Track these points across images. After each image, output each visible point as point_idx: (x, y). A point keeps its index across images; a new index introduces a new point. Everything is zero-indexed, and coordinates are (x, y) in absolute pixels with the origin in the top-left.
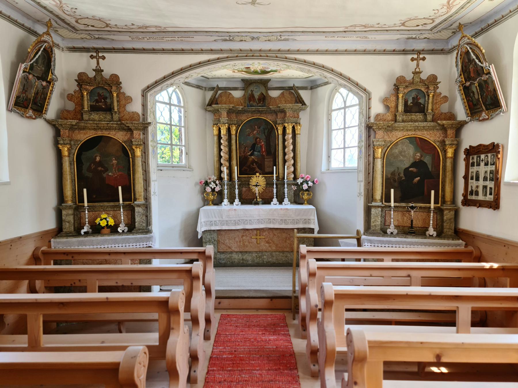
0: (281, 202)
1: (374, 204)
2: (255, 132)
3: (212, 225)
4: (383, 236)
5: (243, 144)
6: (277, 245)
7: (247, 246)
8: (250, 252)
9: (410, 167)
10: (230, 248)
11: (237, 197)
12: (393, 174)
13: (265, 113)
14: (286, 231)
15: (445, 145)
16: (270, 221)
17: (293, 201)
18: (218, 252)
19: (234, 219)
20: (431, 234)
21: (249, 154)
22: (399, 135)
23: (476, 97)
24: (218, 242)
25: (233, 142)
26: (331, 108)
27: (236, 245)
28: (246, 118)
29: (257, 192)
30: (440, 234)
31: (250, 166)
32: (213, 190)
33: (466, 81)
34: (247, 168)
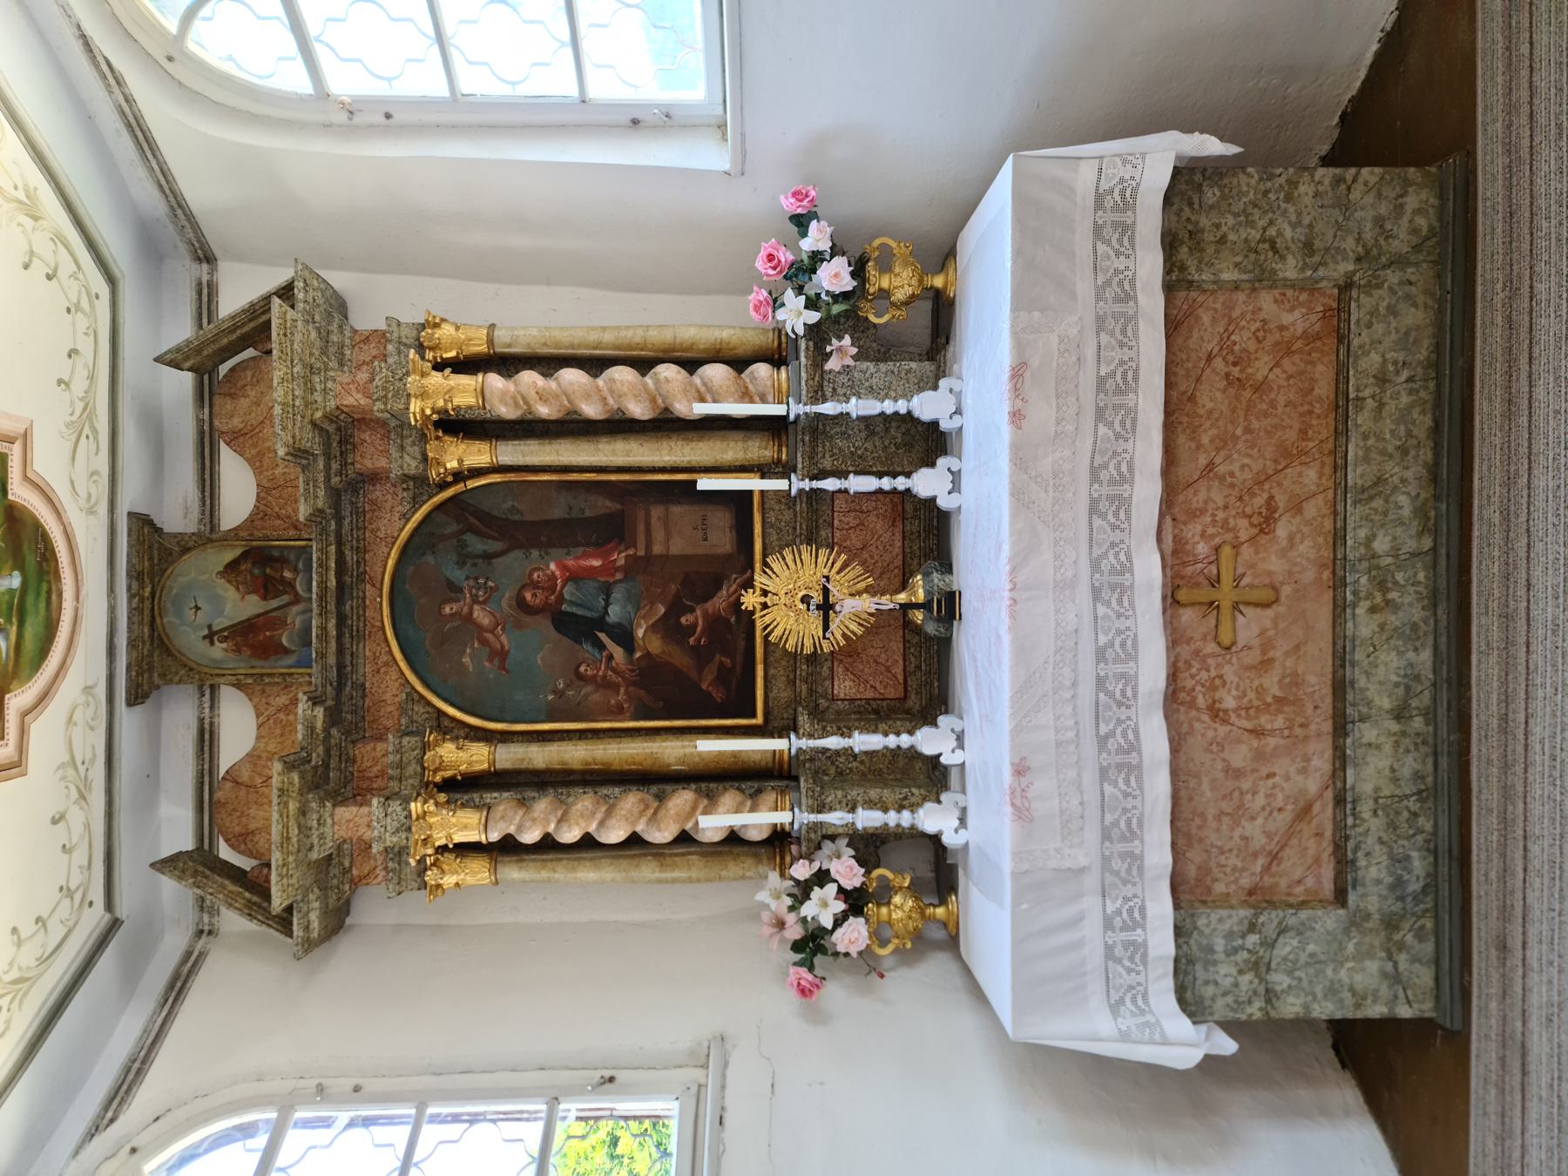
0: (931, 442)
2: (481, 616)
3: (1138, 951)
5: (560, 694)
6: (1287, 455)
7: (1294, 681)
8: (1341, 659)
10: (1304, 813)
11: (905, 740)
13: (361, 550)
14: (1184, 385)
16: (1109, 506)
17: (928, 367)
18: (1340, 897)
19: (1090, 777)
21: (618, 653)
22: (773, 905)
24: (1260, 898)
25: (539, 756)
26: (301, 100)
27: (1282, 766)
28: (390, 675)
29: (867, 604)
31: (696, 649)
32: (855, 901)
34: (712, 670)
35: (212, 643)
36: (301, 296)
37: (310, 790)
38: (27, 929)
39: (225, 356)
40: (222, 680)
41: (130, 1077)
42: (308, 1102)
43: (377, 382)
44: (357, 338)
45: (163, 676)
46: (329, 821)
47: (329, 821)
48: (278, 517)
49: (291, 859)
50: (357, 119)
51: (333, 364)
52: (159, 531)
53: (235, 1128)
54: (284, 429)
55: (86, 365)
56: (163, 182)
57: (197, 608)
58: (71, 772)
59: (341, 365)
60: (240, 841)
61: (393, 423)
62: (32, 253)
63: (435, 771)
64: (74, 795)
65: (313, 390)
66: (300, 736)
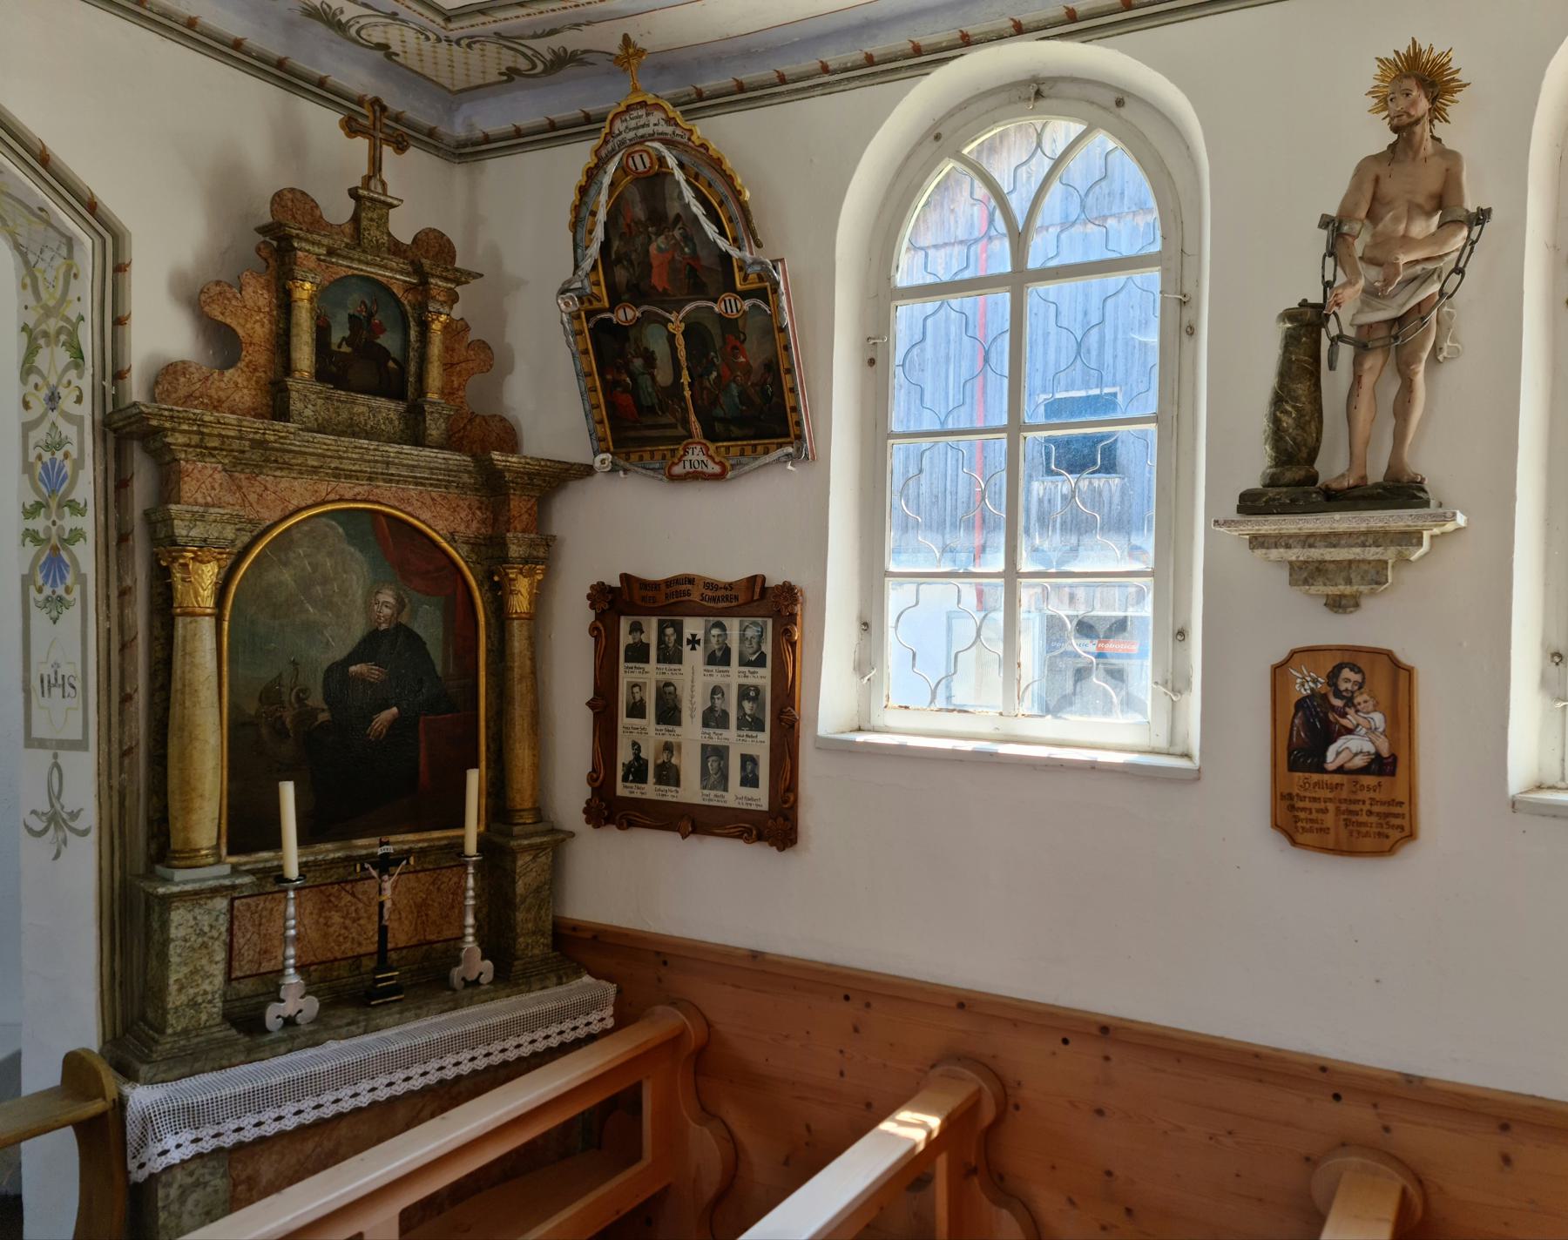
1: (183, 879)
4: (251, 1056)
9: (353, 658)
12: (270, 695)
15: (505, 559)
20: (472, 976)
22: (292, 496)
23: (664, 376)
30: (510, 974)
33: (615, 301)
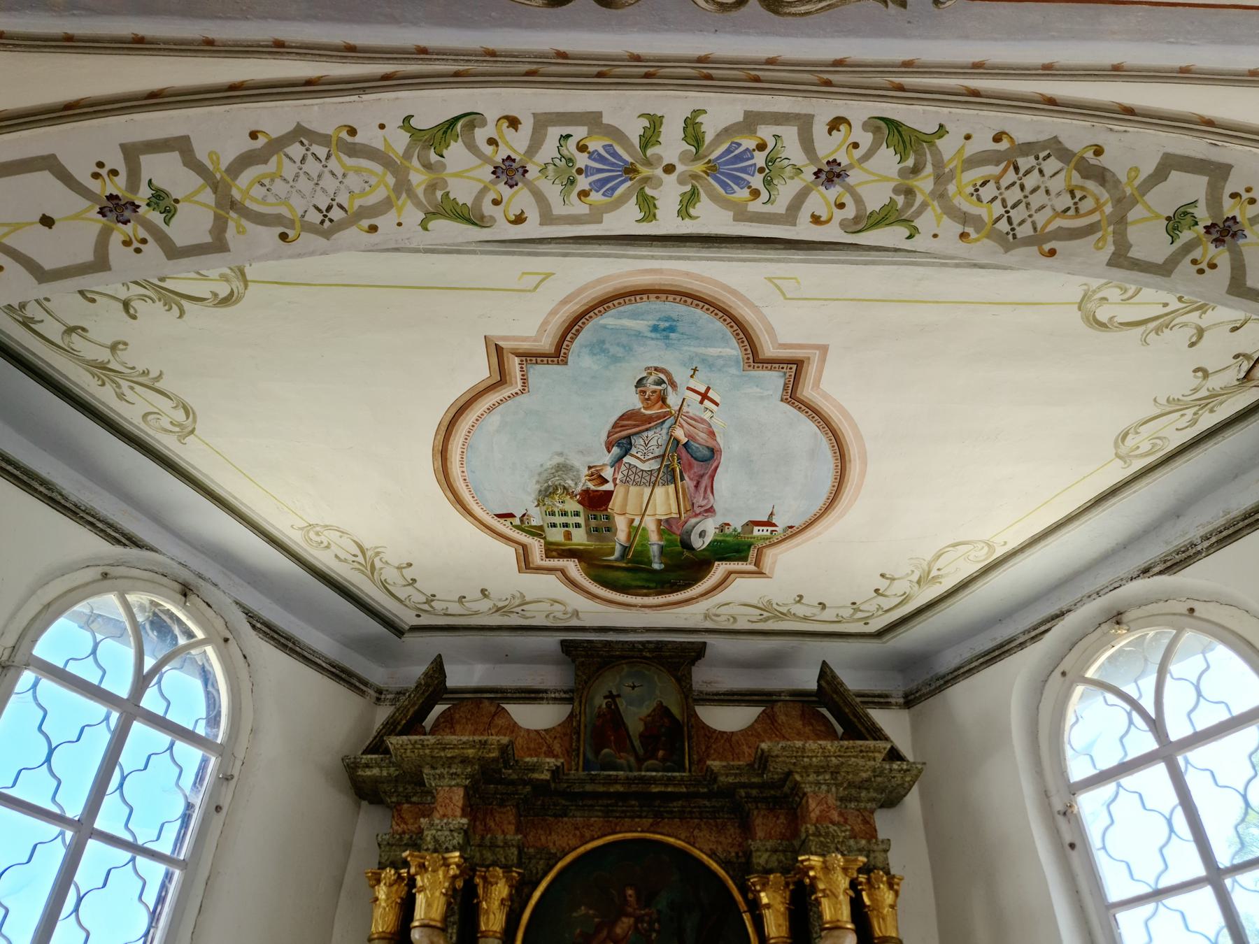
26: (1062, 771)
28: (574, 842)
35: (605, 697)
36: (895, 766)
37: (481, 767)
38: (409, 573)
39: (833, 707)
40: (576, 704)
41: (283, 640)
42: (220, 767)
43: (832, 828)
44: (866, 814)
45: (583, 664)
46: (453, 783)
47: (453, 783)
48: (708, 747)
49: (427, 751)
50: (1061, 820)
51: (842, 792)
52: (693, 662)
53: (219, 713)
54: (783, 748)
55: (815, 615)
56: (962, 670)
57: (633, 687)
58: (517, 602)
59: (841, 799)
60: (447, 721)
61: (796, 843)
62: (893, 579)
63: (484, 878)
64: (500, 604)
65: (818, 773)
66: (528, 759)
